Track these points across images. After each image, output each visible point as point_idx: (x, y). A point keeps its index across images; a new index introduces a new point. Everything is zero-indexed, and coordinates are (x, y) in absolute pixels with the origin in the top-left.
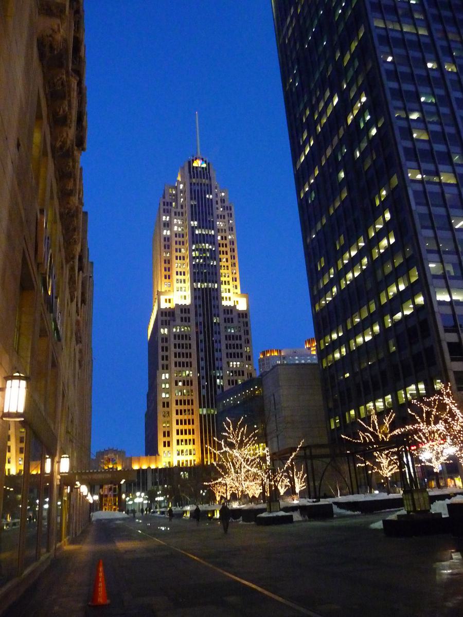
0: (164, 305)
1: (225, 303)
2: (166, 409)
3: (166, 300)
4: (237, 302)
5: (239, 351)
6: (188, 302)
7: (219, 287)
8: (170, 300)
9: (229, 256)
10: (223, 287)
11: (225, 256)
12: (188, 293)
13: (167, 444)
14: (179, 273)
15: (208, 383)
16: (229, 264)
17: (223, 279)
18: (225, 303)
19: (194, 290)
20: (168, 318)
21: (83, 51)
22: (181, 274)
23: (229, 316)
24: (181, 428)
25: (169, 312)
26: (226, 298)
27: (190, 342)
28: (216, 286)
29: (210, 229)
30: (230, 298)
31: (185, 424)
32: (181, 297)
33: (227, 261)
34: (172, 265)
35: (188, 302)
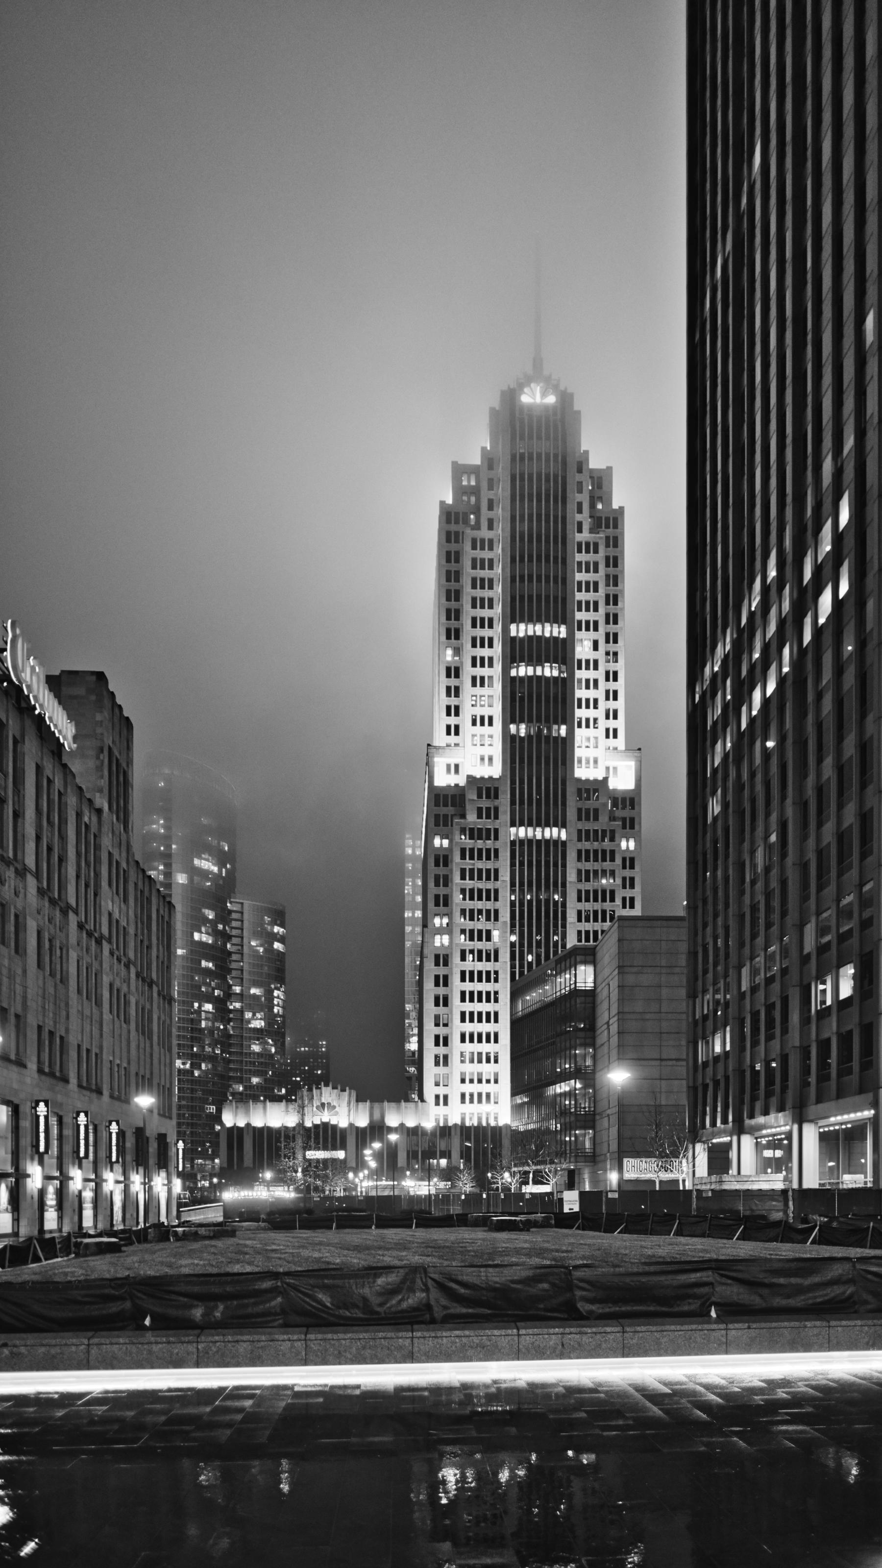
0: (442, 779)
1: (582, 773)
2: (441, 1070)
3: (448, 767)
4: (615, 769)
5: (607, 844)
6: (495, 770)
7: (571, 732)
8: (457, 767)
9: (600, 636)
10: (580, 734)
11: (592, 635)
12: (496, 750)
13: (443, 1061)
14: (467, 1097)
15: (532, 896)
16: (600, 655)
17: (581, 713)
18: (582, 773)
19: (511, 743)
20: (450, 810)
21: (85, 974)
22: (482, 659)
23: (591, 804)
24: (471, 1030)
25: (454, 797)
26: (588, 762)
27: (496, 802)
28: (563, 730)
29: (556, 621)
30: (596, 761)
31: (480, 1000)
32: (482, 759)
33: (596, 647)
34: (451, 1049)
35: (495, 770)
